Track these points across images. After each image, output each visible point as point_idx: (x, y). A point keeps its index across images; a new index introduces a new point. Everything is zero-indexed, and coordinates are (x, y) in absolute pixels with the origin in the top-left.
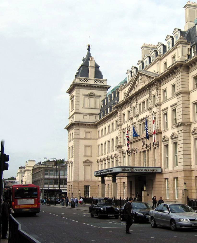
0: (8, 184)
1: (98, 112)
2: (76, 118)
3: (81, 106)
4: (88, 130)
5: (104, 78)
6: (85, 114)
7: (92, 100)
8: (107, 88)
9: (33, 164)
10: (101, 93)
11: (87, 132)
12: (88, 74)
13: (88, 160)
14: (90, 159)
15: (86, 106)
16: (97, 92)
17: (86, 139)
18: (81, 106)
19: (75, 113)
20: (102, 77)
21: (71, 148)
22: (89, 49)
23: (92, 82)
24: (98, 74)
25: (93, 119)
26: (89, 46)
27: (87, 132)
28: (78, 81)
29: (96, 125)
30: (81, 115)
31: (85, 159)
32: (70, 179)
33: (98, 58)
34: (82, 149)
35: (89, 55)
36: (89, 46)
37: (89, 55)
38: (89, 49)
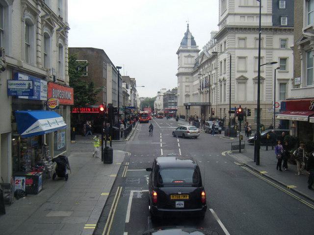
0: (138, 100)
1: (193, 66)
2: (232, 21)
3: (183, 63)
4: (187, 77)
5: (197, 45)
6: (186, 68)
7: (190, 59)
8: (198, 51)
9: (165, 91)
10: (195, 54)
11: (186, 78)
12: (188, 40)
13: (242, 76)
14: (188, 93)
15: (186, 63)
16: (192, 54)
17: (186, 82)
18: (183, 63)
19: (229, 14)
20: (195, 44)
21: (223, 62)
22: (188, 27)
23: (189, 48)
24: (193, 43)
25: (190, 71)
26: (188, 25)
27: (186, 78)
28: (181, 48)
29: (192, 74)
30: (236, 16)
31: (186, 93)
32: (223, 100)
33: (194, 33)
34: (184, 87)
35: (188, 31)
36: (188, 25)
37: (188, 31)
38: (188, 27)
